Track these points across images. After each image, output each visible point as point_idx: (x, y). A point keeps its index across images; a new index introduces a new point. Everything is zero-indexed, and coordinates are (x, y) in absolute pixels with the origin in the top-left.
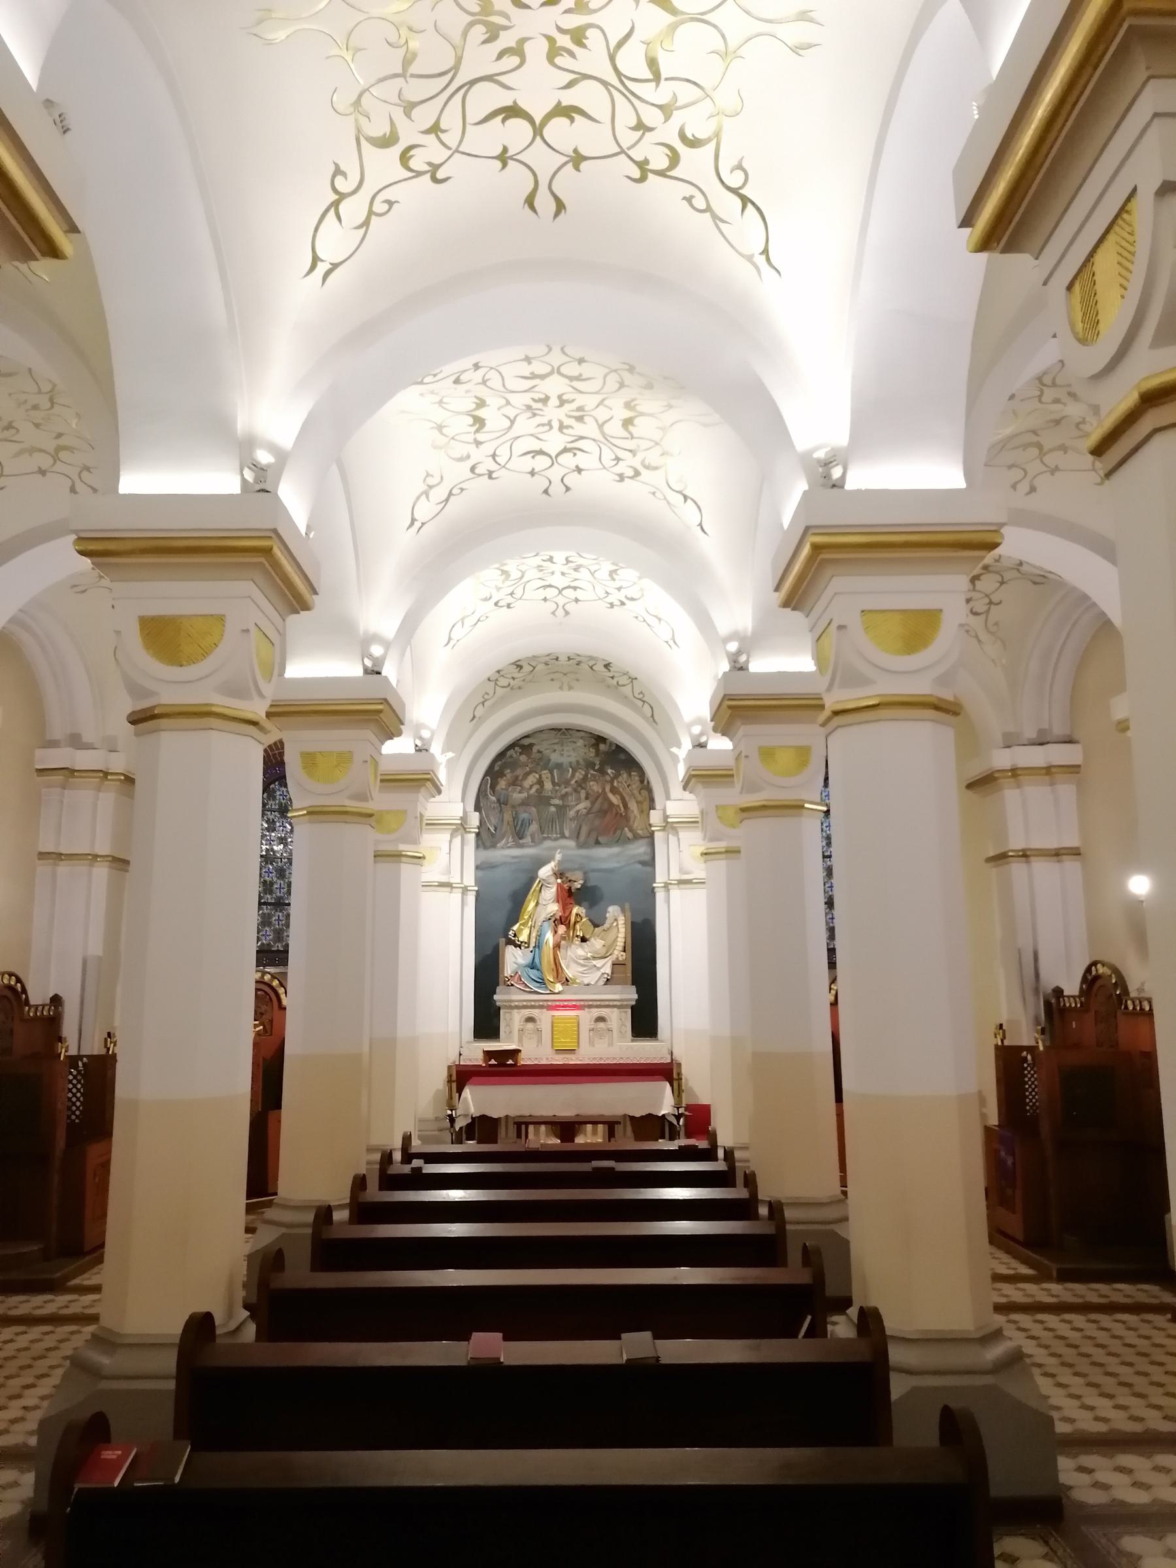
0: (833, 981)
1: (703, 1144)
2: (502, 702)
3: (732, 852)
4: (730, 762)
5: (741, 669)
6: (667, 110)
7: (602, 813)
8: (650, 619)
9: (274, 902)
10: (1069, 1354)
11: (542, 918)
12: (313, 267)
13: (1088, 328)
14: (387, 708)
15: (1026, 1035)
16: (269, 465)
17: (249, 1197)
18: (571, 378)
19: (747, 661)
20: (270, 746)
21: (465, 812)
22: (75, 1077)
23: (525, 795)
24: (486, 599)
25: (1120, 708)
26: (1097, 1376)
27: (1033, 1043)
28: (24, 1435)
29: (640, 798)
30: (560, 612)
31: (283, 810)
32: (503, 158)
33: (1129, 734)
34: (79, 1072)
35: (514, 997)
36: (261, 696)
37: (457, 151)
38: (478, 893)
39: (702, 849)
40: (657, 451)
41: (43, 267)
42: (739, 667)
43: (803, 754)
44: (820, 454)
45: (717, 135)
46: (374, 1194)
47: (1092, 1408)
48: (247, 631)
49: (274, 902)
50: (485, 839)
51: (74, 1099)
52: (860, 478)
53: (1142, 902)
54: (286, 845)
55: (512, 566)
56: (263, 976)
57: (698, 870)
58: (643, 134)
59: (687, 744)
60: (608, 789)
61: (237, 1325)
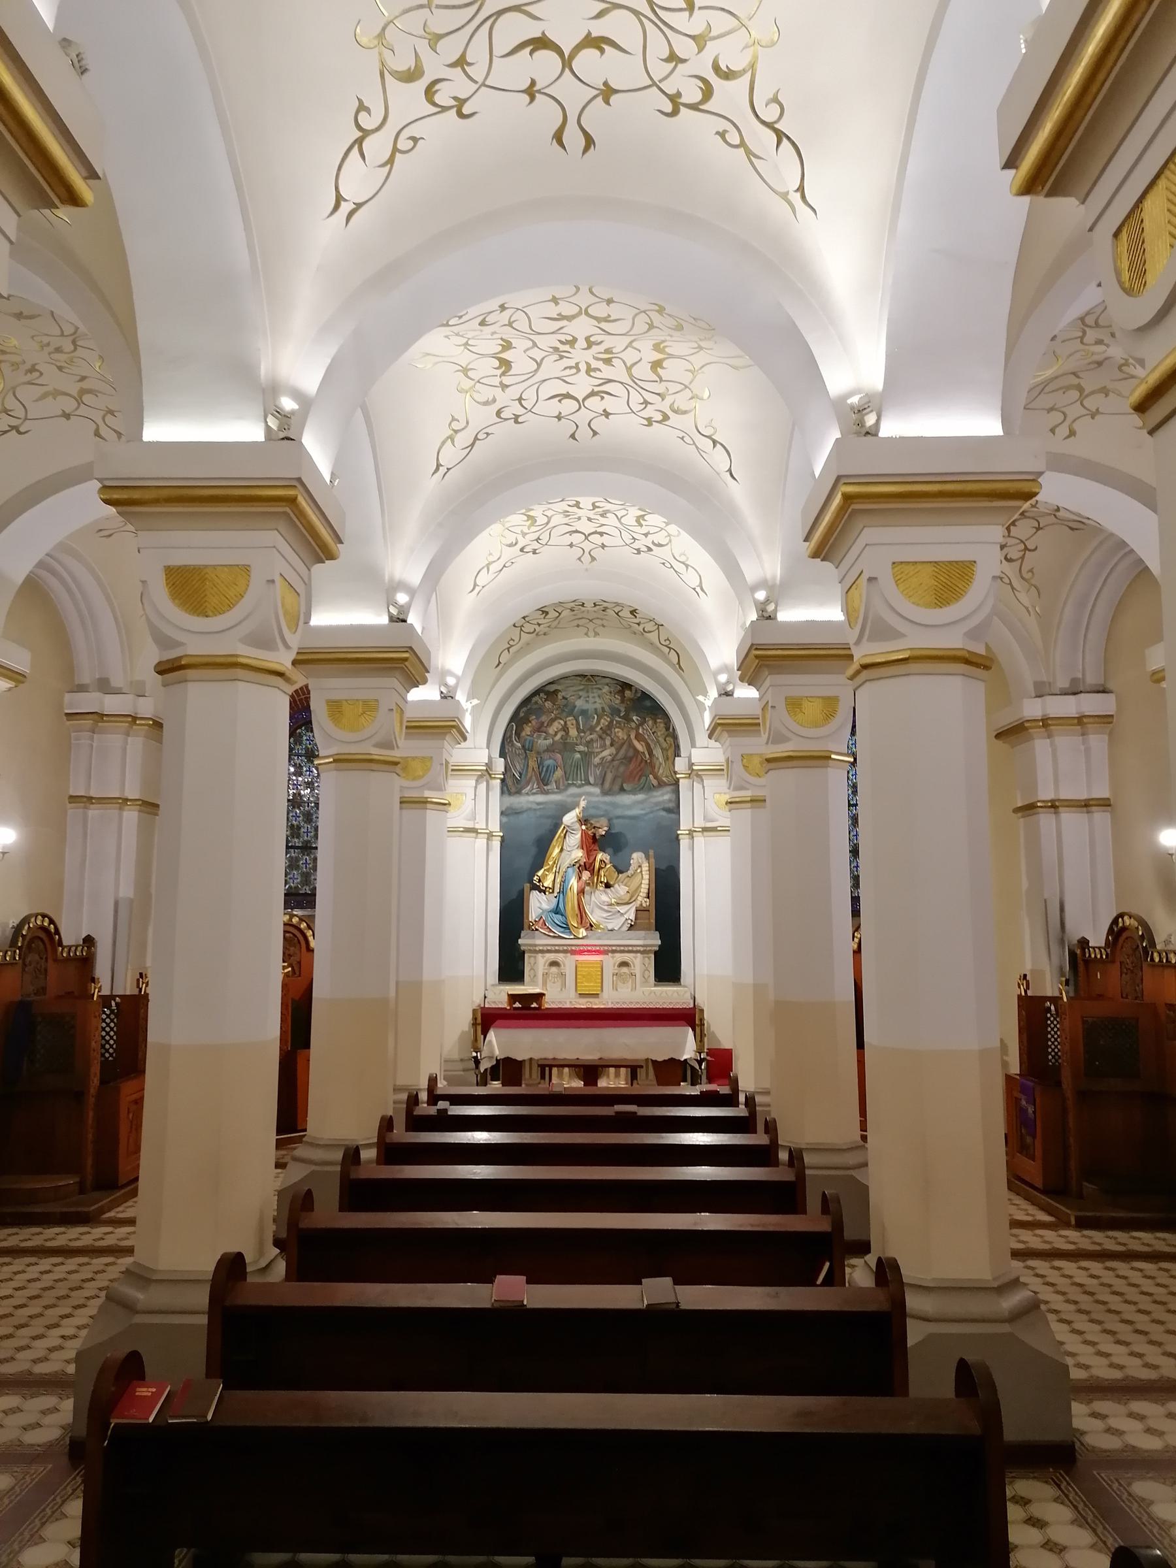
0: (857, 928)
1: (724, 1090)
2: (528, 648)
3: (757, 802)
5: (769, 618)
6: (700, 41)
7: (628, 760)
9: (301, 846)
10: (1085, 1301)
11: (567, 864)
12: (337, 207)
13: (1135, 278)
14: (413, 659)
15: (1050, 985)
16: (293, 412)
17: (278, 1133)
19: (776, 611)
20: (296, 691)
21: (490, 758)
22: (108, 1016)
23: (549, 741)
24: (510, 545)
25: (1156, 658)
26: (1112, 1323)
27: (1057, 994)
29: (665, 745)
30: (586, 558)
31: (311, 755)
32: (531, 92)
33: (1164, 685)
34: (112, 1012)
35: (538, 942)
36: (287, 647)
37: (484, 85)
38: (503, 840)
39: (727, 798)
41: (64, 213)
42: (766, 617)
43: (830, 704)
44: (854, 400)
45: (752, 66)
46: (400, 1134)
48: (273, 581)
49: (301, 846)
50: (510, 785)
51: (107, 1038)
53: (1171, 855)
54: (313, 790)
55: (537, 512)
56: (291, 919)
57: (723, 818)
58: (676, 66)
59: (713, 693)
60: (633, 736)
61: (270, 1269)
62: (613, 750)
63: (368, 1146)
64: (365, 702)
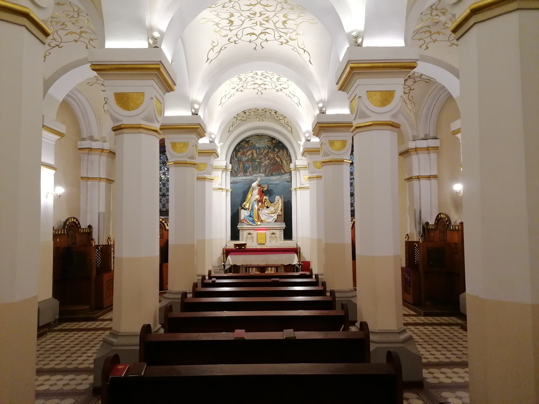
2: (239, 125)
4: (319, 146)
5: (323, 113)
7: (274, 164)
8: (292, 96)
9: (164, 195)
10: (427, 338)
11: (253, 200)
14: (200, 127)
15: (416, 238)
16: (158, 38)
18: (264, 6)
19: (325, 110)
21: (227, 164)
23: (247, 158)
24: (233, 88)
25: (456, 125)
26: (435, 345)
28: (89, 364)
30: (259, 93)
36: (158, 121)
40: (295, 33)
42: (322, 113)
43: (344, 142)
44: (354, 34)
46: (200, 289)
47: (434, 355)
48: (152, 98)
49: (164, 195)
50: (234, 173)
52: (367, 43)
55: (242, 76)
57: (307, 184)
59: (303, 140)
61: (157, 328)
62: (268, 161)
63: (190, 293)
64: (184, 143)
